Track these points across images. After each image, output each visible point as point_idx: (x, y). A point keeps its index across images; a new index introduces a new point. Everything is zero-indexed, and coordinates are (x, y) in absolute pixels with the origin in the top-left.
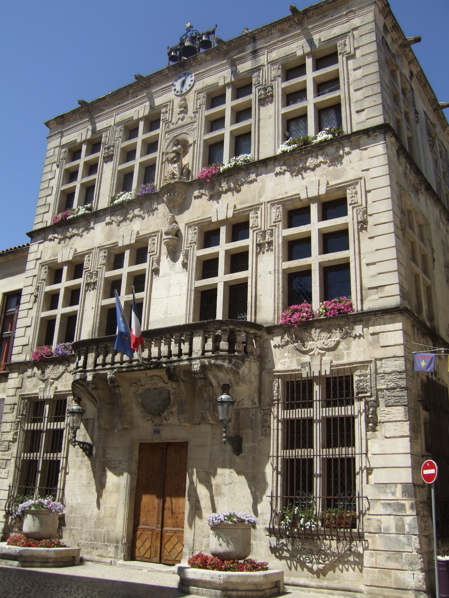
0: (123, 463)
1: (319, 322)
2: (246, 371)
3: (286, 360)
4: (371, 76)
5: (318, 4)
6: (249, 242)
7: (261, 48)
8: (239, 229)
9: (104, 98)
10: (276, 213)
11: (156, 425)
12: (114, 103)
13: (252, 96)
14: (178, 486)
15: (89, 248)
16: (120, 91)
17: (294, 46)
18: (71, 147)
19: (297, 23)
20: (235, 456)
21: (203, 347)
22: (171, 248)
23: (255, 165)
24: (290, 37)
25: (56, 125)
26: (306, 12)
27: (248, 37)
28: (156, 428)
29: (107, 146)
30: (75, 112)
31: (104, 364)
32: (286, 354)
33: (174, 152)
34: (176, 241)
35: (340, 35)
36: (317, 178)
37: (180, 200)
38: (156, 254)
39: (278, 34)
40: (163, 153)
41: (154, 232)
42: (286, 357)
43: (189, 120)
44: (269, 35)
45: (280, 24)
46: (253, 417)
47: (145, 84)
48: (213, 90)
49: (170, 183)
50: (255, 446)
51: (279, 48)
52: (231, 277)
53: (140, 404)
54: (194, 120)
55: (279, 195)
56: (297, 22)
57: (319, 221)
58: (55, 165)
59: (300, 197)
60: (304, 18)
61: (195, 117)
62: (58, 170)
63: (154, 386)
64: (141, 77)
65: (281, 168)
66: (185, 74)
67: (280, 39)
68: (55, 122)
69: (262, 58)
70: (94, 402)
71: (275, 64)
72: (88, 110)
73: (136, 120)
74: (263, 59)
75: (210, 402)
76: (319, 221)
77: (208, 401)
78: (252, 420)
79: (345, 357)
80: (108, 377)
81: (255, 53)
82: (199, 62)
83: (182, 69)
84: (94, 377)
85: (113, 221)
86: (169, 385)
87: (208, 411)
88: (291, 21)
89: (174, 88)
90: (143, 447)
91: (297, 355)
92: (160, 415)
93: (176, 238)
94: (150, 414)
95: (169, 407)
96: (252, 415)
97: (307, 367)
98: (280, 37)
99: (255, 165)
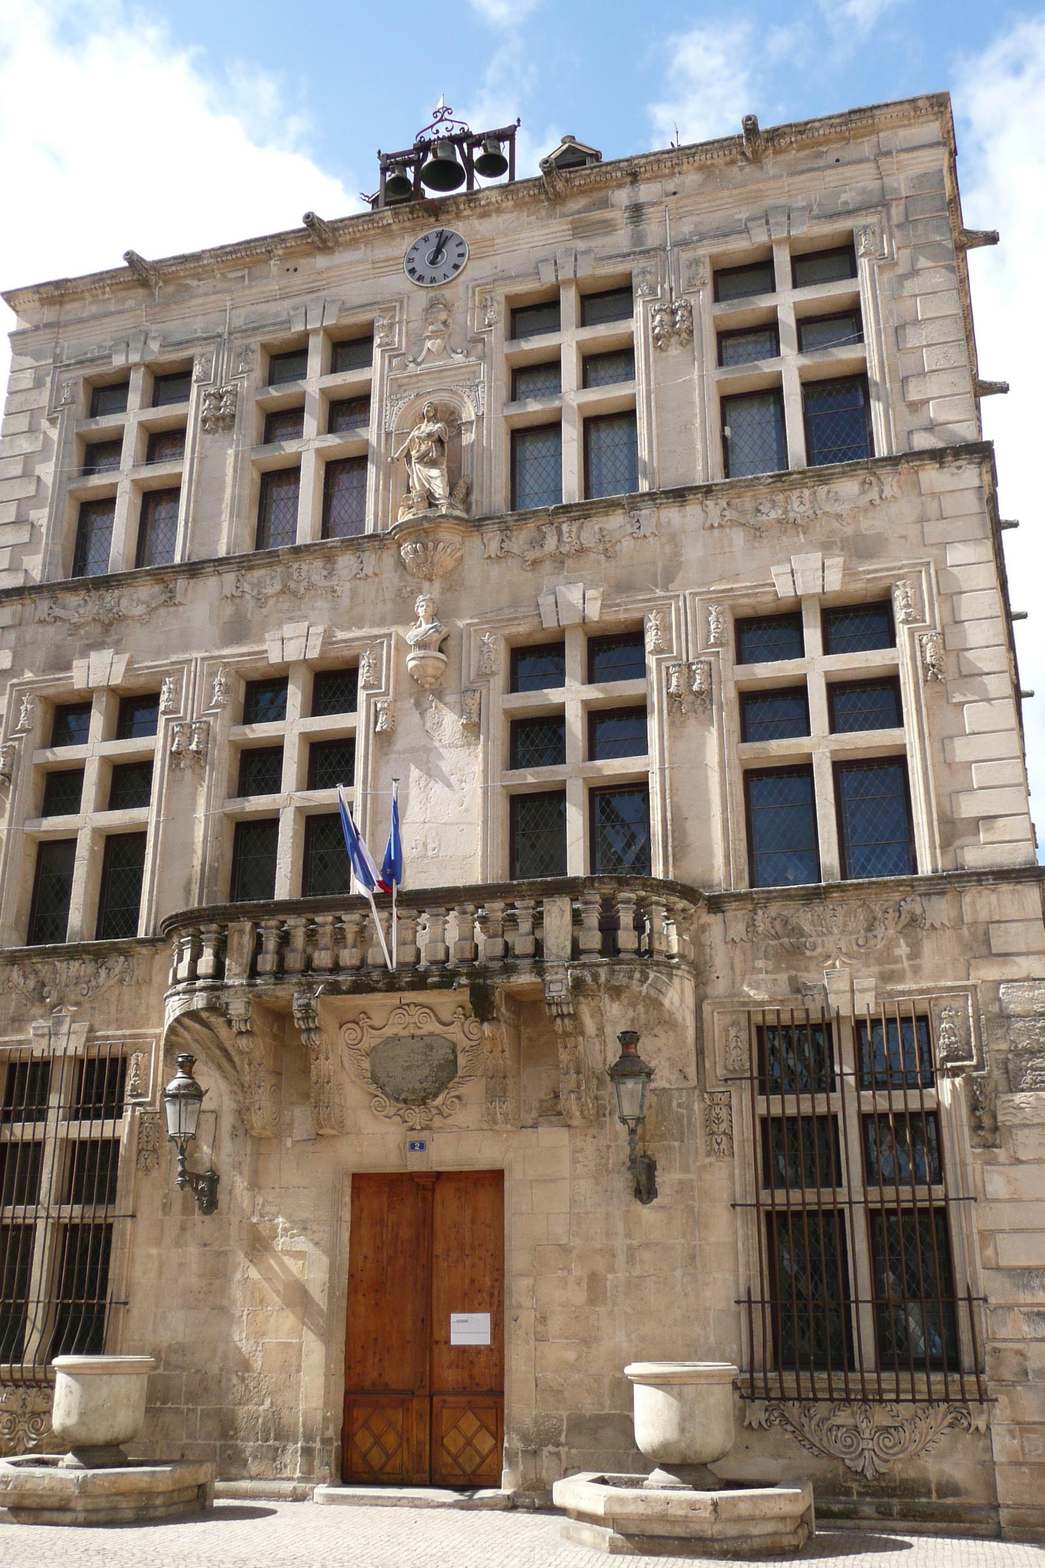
0: (315, 1227)
1: (843, 891)
2: (676, 1000)
3: (761, 976)
4: (941, 322)
6: (155, 744)
8: (135, 709)
10: (719, 625)
11: (412, 1129)
14: (473, 1281)
19: (747, 159)
25: (37, 304)
26: (775, 134)
27: (621, 169)
28: (415, 1136)
31: (281, 972)
32: (760, 964)
33: (430, 435)
34: (441, 665)
40: (388, 434)
42: (760, 971)
44: (673, 174)
55: (720, 580)
56: (749, 155)
57: (303, 716)
60: (766, 148)
63: (411, 1030)
64: (141, 260)
70: (226, 1065)
75: (578, 1072)
76: (303, 716)
77: (572, 1071)
78: (679, 1119)
79: (909, 974)
82: (479, 210)
83: (432, 220)
87: (573, 1096)
90: (362, 1182)
91: (790, 967)
92: (425, 1104)
94: (397, 1100)
95: (451, 1085)
96: (679, 1105)
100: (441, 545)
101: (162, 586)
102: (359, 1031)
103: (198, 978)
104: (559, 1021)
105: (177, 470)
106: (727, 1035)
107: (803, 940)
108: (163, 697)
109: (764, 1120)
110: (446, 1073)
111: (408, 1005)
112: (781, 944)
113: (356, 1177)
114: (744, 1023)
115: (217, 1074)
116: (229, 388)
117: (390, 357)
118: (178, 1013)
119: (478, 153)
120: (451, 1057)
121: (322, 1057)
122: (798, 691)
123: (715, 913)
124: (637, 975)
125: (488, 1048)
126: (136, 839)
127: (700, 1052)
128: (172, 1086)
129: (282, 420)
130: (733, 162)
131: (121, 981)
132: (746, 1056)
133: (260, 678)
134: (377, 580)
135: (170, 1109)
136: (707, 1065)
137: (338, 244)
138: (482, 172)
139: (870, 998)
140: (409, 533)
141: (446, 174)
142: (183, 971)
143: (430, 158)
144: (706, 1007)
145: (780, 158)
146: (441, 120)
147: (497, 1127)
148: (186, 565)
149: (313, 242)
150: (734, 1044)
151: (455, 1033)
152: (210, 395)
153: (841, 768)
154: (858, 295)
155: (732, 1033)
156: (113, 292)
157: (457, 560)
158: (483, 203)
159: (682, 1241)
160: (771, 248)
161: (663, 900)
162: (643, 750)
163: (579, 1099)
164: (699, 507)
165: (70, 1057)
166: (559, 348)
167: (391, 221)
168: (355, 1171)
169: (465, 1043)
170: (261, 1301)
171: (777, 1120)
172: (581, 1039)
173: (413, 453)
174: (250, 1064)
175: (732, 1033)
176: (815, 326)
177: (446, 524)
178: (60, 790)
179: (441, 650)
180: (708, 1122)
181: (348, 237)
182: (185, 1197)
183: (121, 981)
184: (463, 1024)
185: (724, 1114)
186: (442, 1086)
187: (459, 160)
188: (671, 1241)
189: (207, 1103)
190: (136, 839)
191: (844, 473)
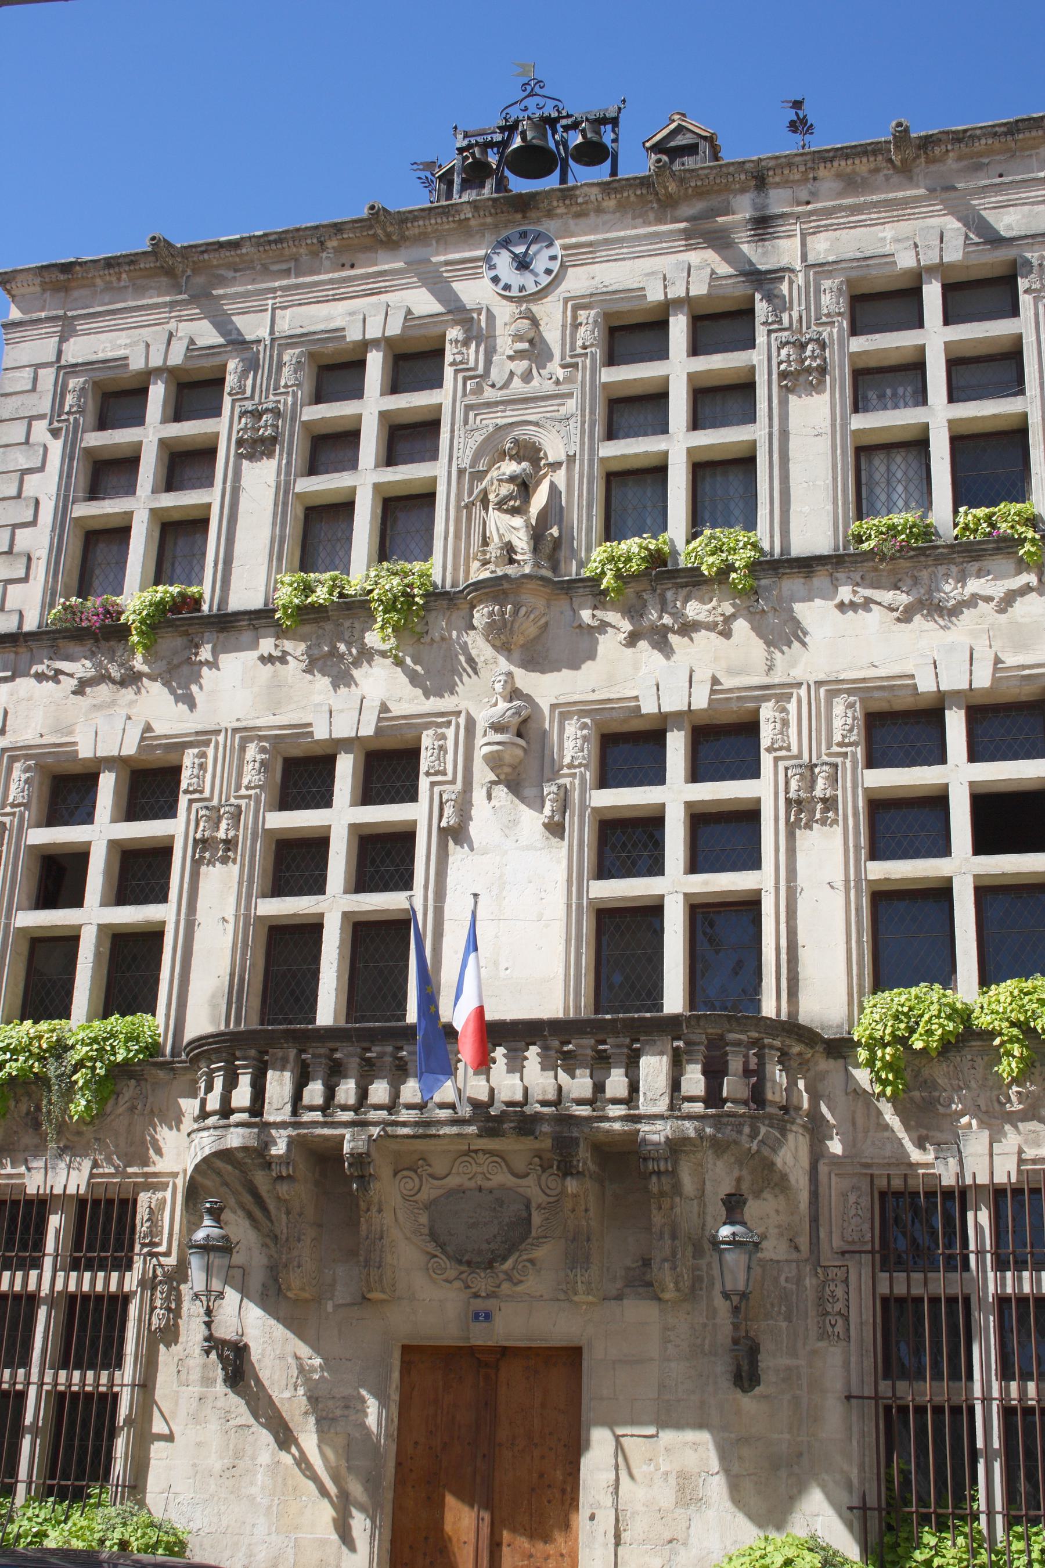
5: (965, 131)
6: (174, 829)
7: (781, 216)
9: (235, 245)
10: (844, 719)
11: (476, 1296)
12: (265, 268)
13: (756, 357)
14: (541, 1475)
15: (200, 727)
16: (296, 235)
17: (888, 232)
18: (100, 376)
19: (894, 166)
20: (739, 1394)
21: (675, 1085)
22: (507, 770)
23: (776, 569)
24: (874, 205)
25: (38, 289)
26: (927, 142)
28: (479, 1304)
29: (249, 405)
30: (119, 265)
33: (512, 479)
34: (520, 752)
35: (1026, 237)
36: (966, 641)
37: (532, 631)
38: (453, 782)
39: (837, 185)
40: (461, 472)
41: (442, 714)
43: (549, 387)
44: (807, 180)
45: (847, 157)
46: (789, 1286)
47: (388, 235)
48: (625, 306)
49: (506, 577)
50: (798, 1367)
51: (839, 227)
52: (706, 883)
53: (426, 1231)
54: (564, 388)
57: (353, 804)
58: (40, 429)
59: (915, 686)
60: (918, 157)
61: (568, 380)
62: (56, 447)
65: (855, 592)
66: (523, 235)
67: (845, 202)
68: (38, 281)
69: (783, 243)
70: (258, 1214)
71: (829, 275)
72: (177, 269)
73: (355, 343)
74: (785, 251)
75: (674, 1237)
77: (666, 1236)
80: (346, 1148)
81: (763, 225)
82: (575, 209)
83: (519, 216)
84: (291, 1142)
85: (285, 653)
86: (530, 1181)
88: (880, 158)
89: (492, 273)
90: (414, 1356)
93: (521, 741)
94: (460, 1262)
96: (787, 1280)
97: (951, 1160)
98: (840, 195)
99: (776, 569)
100: (523, 610)
101: (185, 639)
102: (417, 1180)
103: (233, 1112)
104: (654, 1179)
105: (205, 500)
106: (846, 1201)
107: (936, 1094)
108: (185, 774)
109: (885, 1300)
110: (517, 1234)
111: (476, 1151)
112: (912, 1099)
113: (407, 1350)
114: (865, 1186)
115: (246, 1223)
116: (271, 405)
117: (465, 379)
118: (207, 1151)
119: (576, 139)
120: (525, 1214)
121: (374, 1209)
122: (937, 801)
123: (835, 1058)
124: (747, 1130)
125: (570, 1206)
126: (150, 939)
127: (814, 1220)
128: (200, 1235)
129: (332, 447)
130: (877, 170)
131: (133, 1108)
132: (866, 1227)
133: (302, 755)
134: (444, 645)
135: (196, 1263)
136: (822, 1235)
137: (404, 238)
138: (577, 161)
139: (1012, 1165)
140: (486, 594)
141: (535, 161)
142: (213, 1102)
143: (517, 142)
144: (823, 1169)
145: (933, 168)
146: (529, 96)
147: (576, 1298)
148: (216, 616)
149: (374, 235)
150: (853, 1212)
151: (530, 1187)
152: (246, 412)
153: (986, 893)
154: (1020, 337)
155: (852, 1199)
156: (130, 279)
157: (540, 628)
158: (580, 200)
159: (787, 1436)
160: (920, 276)
161: (777, 1043)
162: (755, 863)
163: (674, 1268)
164: (828, 580)
165: (71, 1196)
166: (666, 379)
167: (470, 215)
168: (406, 1342)
169: (541, 1199)
170: (295, 1489)
171: (901, 1301)
172: (677, 1199)
173: (492, 497)
174: (288, 1213)
175: (852, 1199)
176: (971, 373)
177: (531, 585)
178: (58, 878)
179: (519, 734)
180: (821, 1300)
181: (417, 231)
182: (205, 1366)
183: (133, 1108)
184: (539, 1178)
185: (840, 1292)
186: (512, 1248)
187: (552, 145)
188: (776, 1436)
189: (237, 1259)
190: (150, 939)
191: (998, 549)
